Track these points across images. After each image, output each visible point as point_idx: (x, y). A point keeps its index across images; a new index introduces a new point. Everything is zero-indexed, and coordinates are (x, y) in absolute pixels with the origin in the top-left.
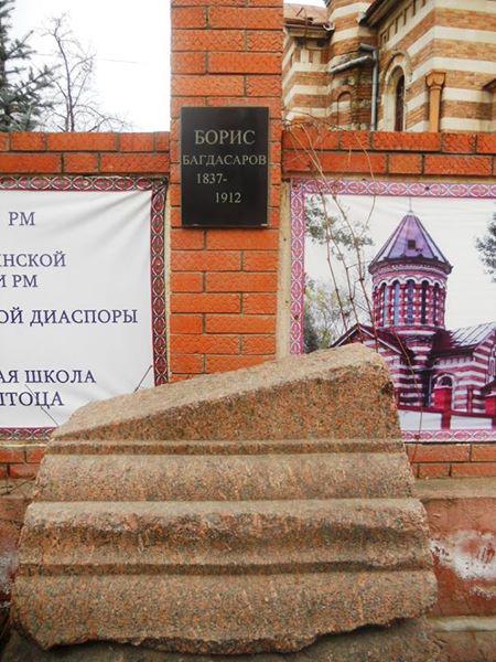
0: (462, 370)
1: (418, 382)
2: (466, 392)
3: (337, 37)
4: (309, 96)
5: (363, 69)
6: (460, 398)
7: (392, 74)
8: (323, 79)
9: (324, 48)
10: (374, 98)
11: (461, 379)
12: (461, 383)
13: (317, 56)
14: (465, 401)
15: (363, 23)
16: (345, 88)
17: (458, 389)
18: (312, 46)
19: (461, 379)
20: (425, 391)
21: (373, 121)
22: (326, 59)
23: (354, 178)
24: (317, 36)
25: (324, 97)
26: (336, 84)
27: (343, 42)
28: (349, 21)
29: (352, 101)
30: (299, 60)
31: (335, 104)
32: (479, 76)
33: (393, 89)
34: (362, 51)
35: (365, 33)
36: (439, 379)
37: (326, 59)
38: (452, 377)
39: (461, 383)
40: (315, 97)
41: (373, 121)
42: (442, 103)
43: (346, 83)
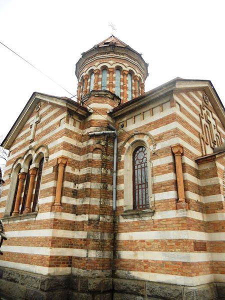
0: (156, 124)
1: (95, 150)
2: (170, 159)
3: (94, 117)
4: (72, 145)
5: (111, 138)
6: (159, 170)
7: (132, 144)
8: (81, 138)
9: (82, 122)
10: (115, 156)
11: (160, 138)
12: (159, 146)
13: (78, 124)
14: (172, 195)
15: (110, 114)
16: (98, 146)
17: (155, 155)
18: (76, 118)
19: (160, 138)
20: (105, 164)
21: (115, 169)
22: (83, 127)
23: (113, 237)
24: (81, 113)
25: (80, 148)
26: (91, 142)
27: (97, 120)
28: (102, 111)
29: (102, 154)
30: (68, 123)
31: (90, 154)
32: (196, 156)
33: (131, 152)
34: (109, 128)
35: (110, 119)
36: (127, 145)
37: (83, 127)
38: (145, 139)
39: (159, 146)
40: (75, 147)
41: (115, 169)
42: (177, 189)
43: (99, 143)
